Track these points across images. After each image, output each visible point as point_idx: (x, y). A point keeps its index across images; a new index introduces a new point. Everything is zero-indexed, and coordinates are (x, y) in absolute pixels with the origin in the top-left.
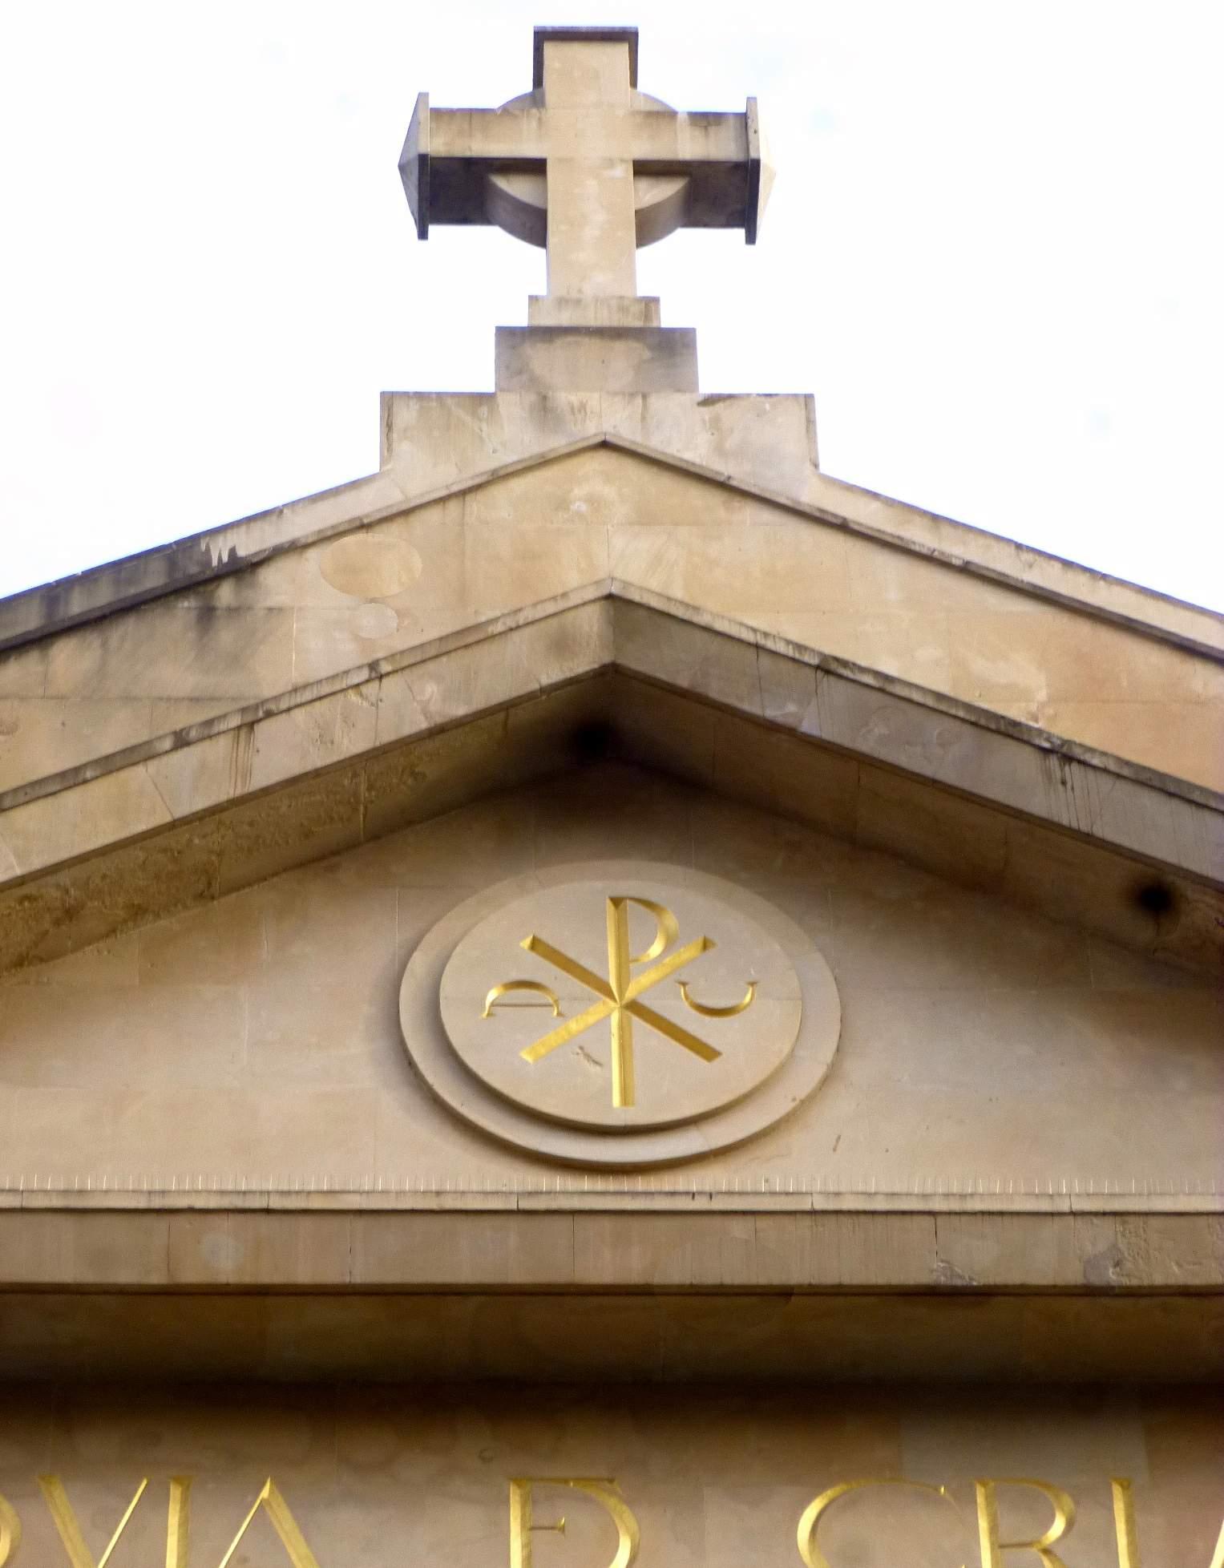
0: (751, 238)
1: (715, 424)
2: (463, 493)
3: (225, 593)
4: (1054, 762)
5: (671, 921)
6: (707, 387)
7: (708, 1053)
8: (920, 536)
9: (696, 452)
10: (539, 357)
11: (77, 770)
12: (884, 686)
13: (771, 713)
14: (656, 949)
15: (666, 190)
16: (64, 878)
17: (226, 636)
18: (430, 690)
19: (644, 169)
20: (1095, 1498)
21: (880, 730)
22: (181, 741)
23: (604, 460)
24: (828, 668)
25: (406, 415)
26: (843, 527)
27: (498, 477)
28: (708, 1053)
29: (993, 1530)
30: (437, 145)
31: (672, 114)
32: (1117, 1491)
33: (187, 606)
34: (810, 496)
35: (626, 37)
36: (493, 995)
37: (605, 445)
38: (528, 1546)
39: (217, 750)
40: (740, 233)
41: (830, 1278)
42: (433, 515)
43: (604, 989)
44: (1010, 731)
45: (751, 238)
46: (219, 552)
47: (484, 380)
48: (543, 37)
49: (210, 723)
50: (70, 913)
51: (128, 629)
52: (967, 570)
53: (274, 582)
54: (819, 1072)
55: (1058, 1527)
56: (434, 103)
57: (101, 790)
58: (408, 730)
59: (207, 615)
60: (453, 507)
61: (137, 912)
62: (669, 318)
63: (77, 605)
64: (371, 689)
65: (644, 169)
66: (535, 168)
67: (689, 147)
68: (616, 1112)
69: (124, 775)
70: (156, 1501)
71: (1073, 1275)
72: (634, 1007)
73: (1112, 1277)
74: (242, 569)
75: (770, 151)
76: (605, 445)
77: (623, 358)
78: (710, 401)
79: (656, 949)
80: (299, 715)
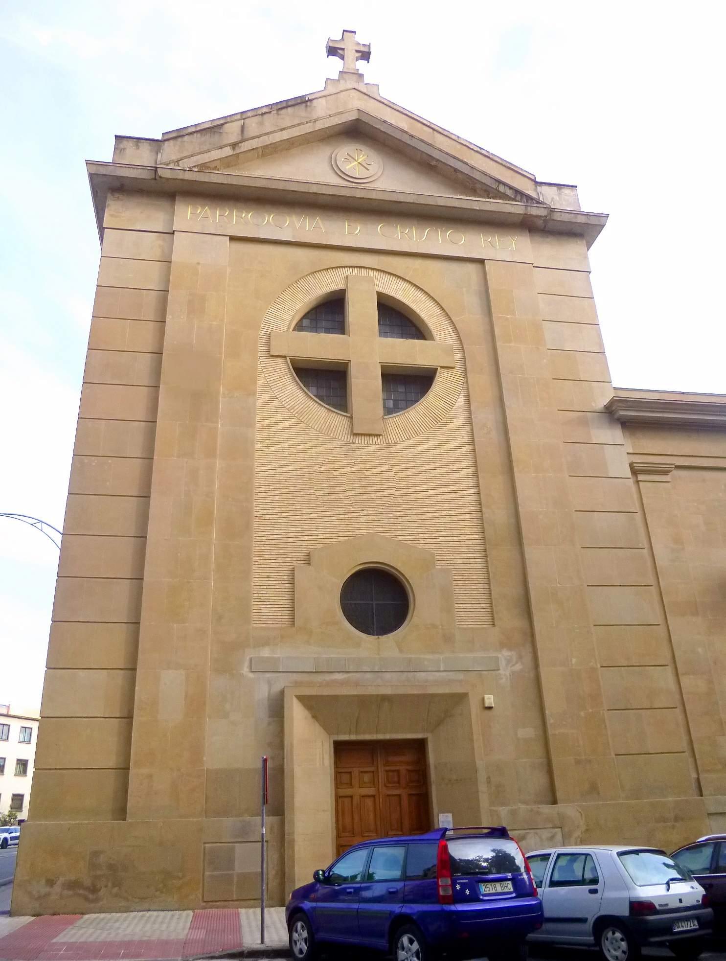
0: (368, 62)
1: (367, 87)
2: (337, 93)
3: (309, 103)
4: (411, 137)
5: (363, 153)
6: (366, 82)
7: (368, 170)
8: (393, 106)
9: (365, 91)
10: (345, 76)
11: (294, 125)
12: (391, 125)
13: (377, 127)
14: (362, 156)
15: (360, 54)
16: (293, 139)
17: (309, 109)
18: (337, 119)
19: (357, 51)
20: (248, 212)
21: (391, 131)
22: (307, 123)
23: (354, 90)
24: (385, 122)
25: (329, 81)
26: (383, 103)
27: (342, 91)
28: (368, 170)
29: (236, 216)
30: (331, 44)
31: (360, 44)
32: (439, 230)
33: (304, 105)
34: (379, 98)
35: (354, 32)
36: (343, 160)
37: (354, 89)
38: (348, 228)
39: (312, 124)
40: (367, 61)
41: (384, 199)
42: (333, 96)
43: (356, 160)
44: (406, 132)
45: (368, 62)
46: (307, 98)
47: (337, 78)
48: (344, 31)
49: (311, 120)
50: (293, 144)
51: (297, 107)
52: (398, 111)
53: (315, 102)
54: (381, 173)
55: (244, 215)
56: (331, 38)
57: (298, 128)
58: (334, 124)
59: (306, 106)
60: (336, 95)
61: (300, 145)
62: (360, 72)
63: (290, 103)
64: (330, 118)
65: (357, 51)
66: (343, 49)
67: (362, 49)
68: (357, 176)
69: (300, 126)
70: (305, 218)
71: (412, 201)
72: (359, 163)
73: (416, 202)
74: (311, 101)
75: (372, 50)
76: (354, 89)
77: (355, 77)
78: (366, 84)
79: (362, 156)
80: (321, 121)
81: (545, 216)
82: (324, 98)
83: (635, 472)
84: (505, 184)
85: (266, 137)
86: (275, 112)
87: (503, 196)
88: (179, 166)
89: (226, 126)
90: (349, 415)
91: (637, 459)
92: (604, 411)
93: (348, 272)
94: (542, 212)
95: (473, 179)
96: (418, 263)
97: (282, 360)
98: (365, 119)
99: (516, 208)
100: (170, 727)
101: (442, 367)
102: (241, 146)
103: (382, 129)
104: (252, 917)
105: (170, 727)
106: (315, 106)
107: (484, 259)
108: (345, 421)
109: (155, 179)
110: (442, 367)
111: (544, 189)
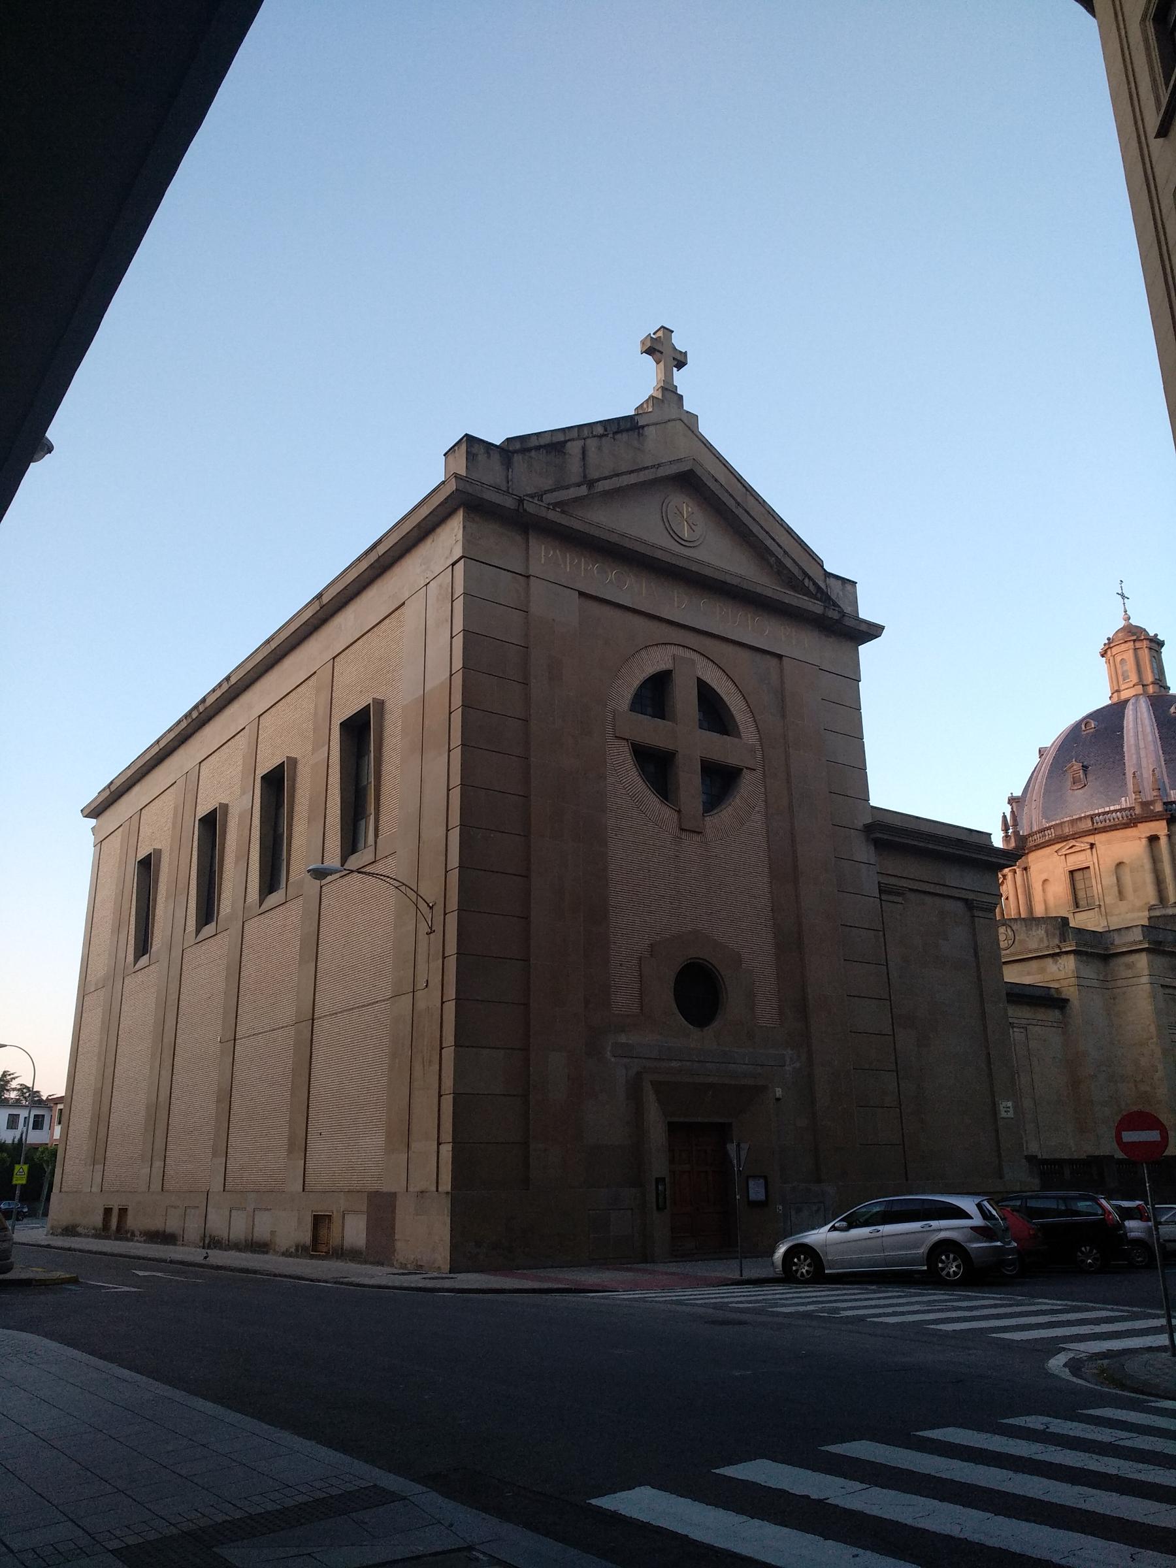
76: (680, 420)
81: (837, 620)
82: (654, 426)
83: (881, 892)
84: (810, 578)
85: (617, 478)
86: (611, 435)
87: (807, 592)
88: (542, 501)
89: (569, 444)
90: (678, 809)
91: (885, 880)
92: (862, 829)
93: (680, 652)
94: (835, 615)
95: (1060, 841)
96: (729, 649)
97: (624, 743)
98: (699, 472)
99: (817, 607)
100: (10, 1261)
101: (747, 768)
102: (598, 486)
103: (712, 487)
104: (1136, 915)
105: (10, 1261)
106: (646, 436)
107: (783, 656)
108: (676, 815)
109: (518, 510)
110: (747, 768)
111: (832, 581)
